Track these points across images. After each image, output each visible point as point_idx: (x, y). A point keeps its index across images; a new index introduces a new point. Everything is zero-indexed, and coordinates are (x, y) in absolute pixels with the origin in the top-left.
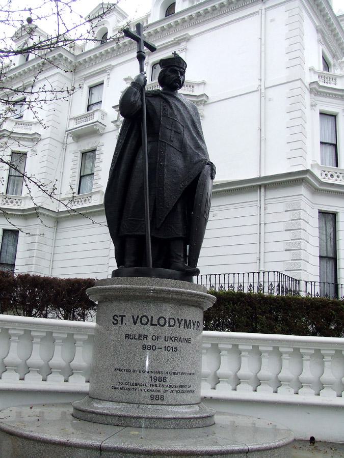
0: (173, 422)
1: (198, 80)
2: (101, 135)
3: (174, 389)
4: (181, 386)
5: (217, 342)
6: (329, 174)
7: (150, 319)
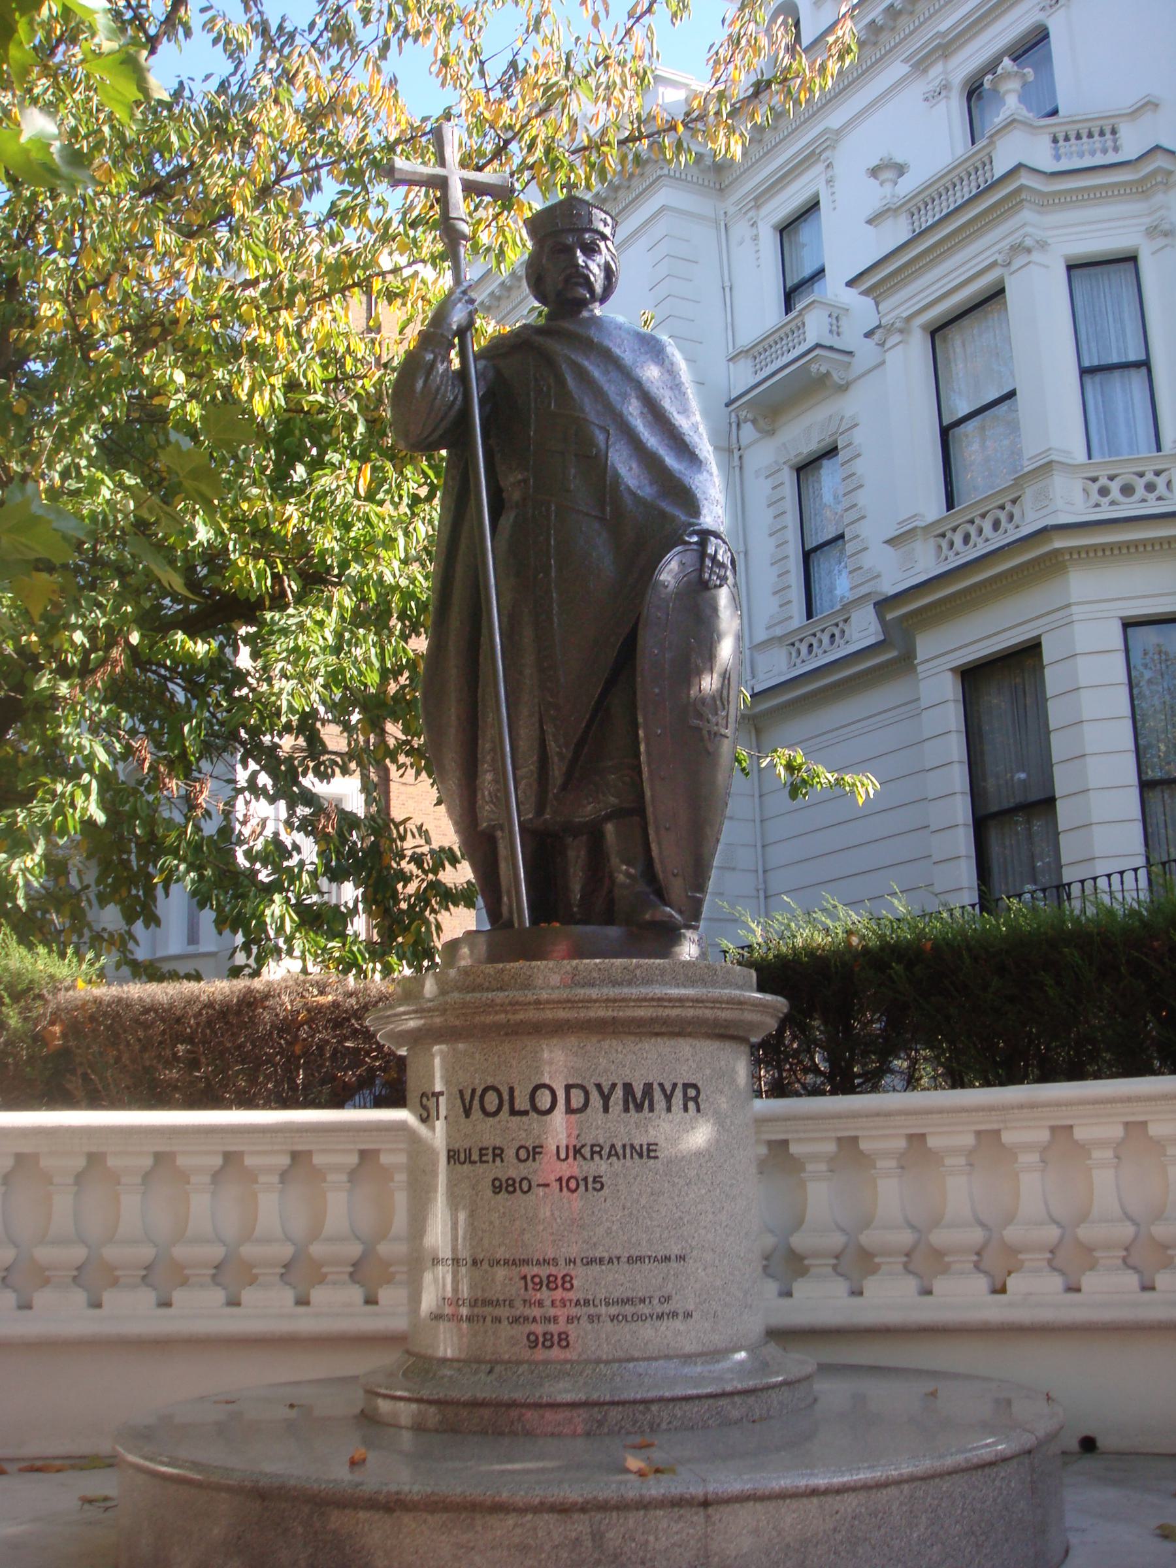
0: (583, 1413)
1: (1127, 100)
2: (844, 388)
3: (603, 1310)
4: (628, 1301)
6: (1115, 487)
7: (506, 1097)
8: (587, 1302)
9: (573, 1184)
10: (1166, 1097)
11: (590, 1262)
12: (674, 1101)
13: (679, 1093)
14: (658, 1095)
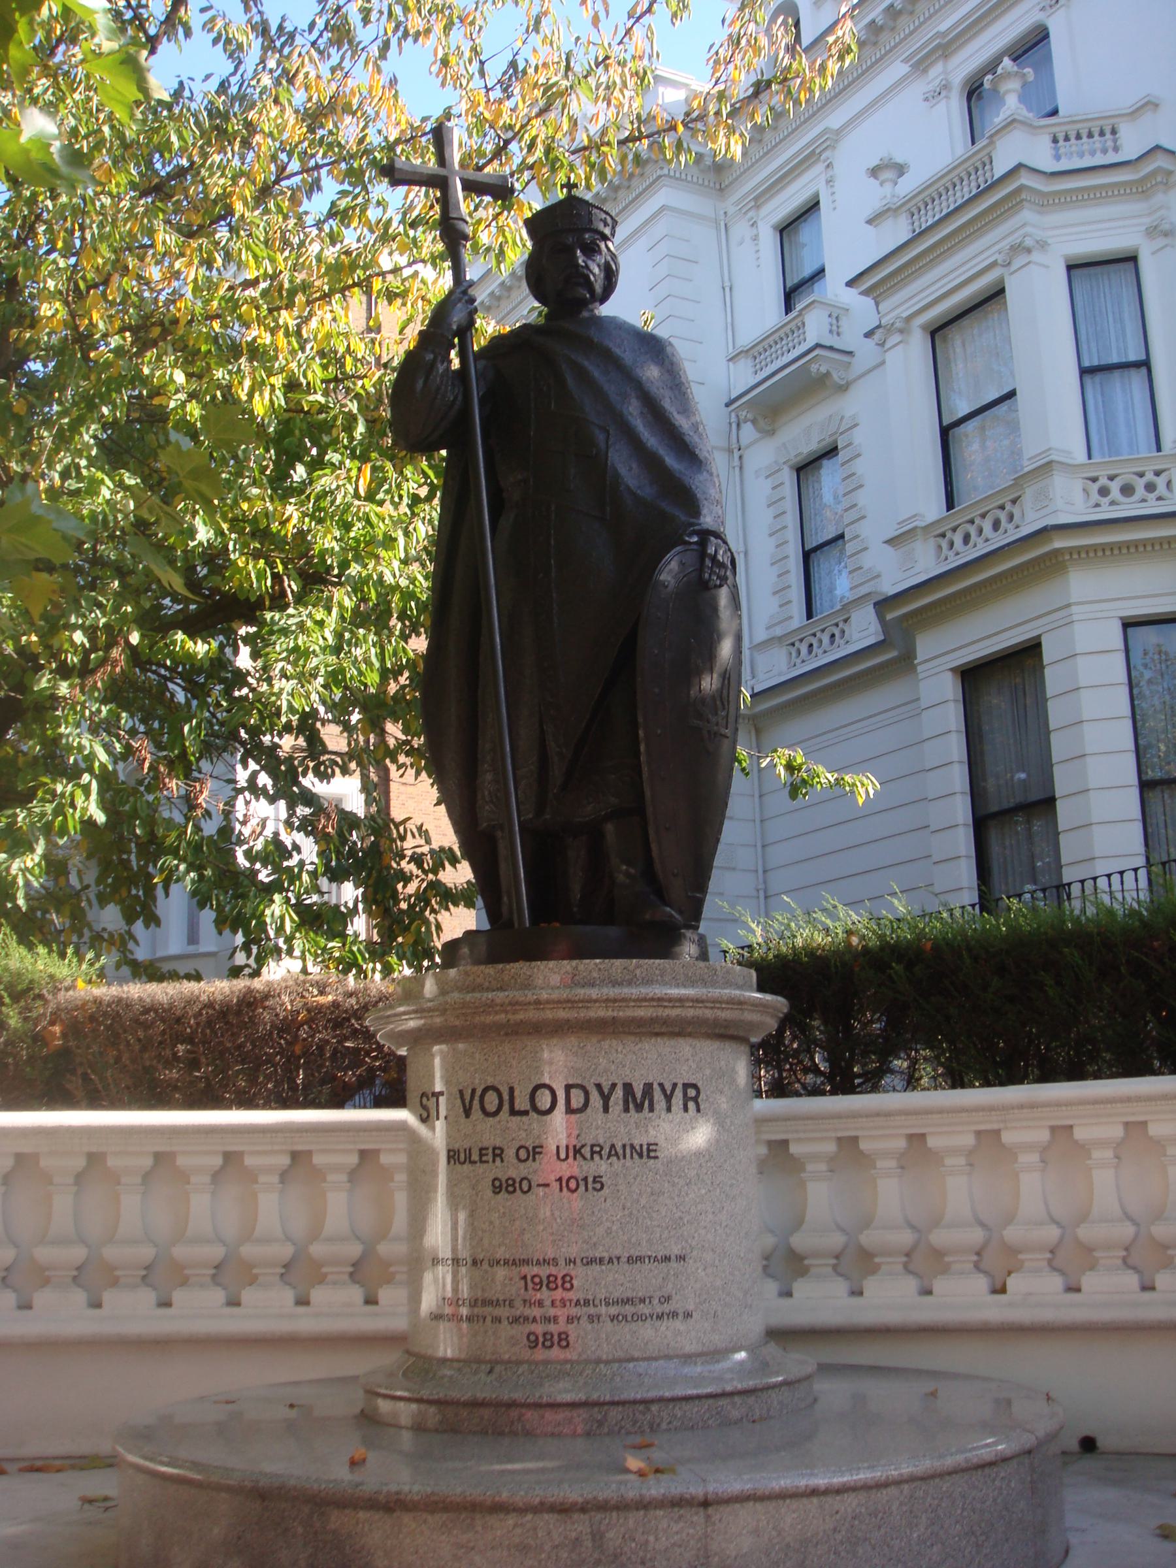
0: (583, 1413)
1: (1127, 100)
2: (844, 388)
3: (603, 1310)
4: (628, 1301)
5: (995, 1126)
6: (1115, 487)
7: (506, 1097)
8: (587, 1303)
9: (573, 1184)
10: (1166, 1097)
11: (590, 1262)
12: (674, 1101)
13: (679, 1093)
14: (658, 1095)
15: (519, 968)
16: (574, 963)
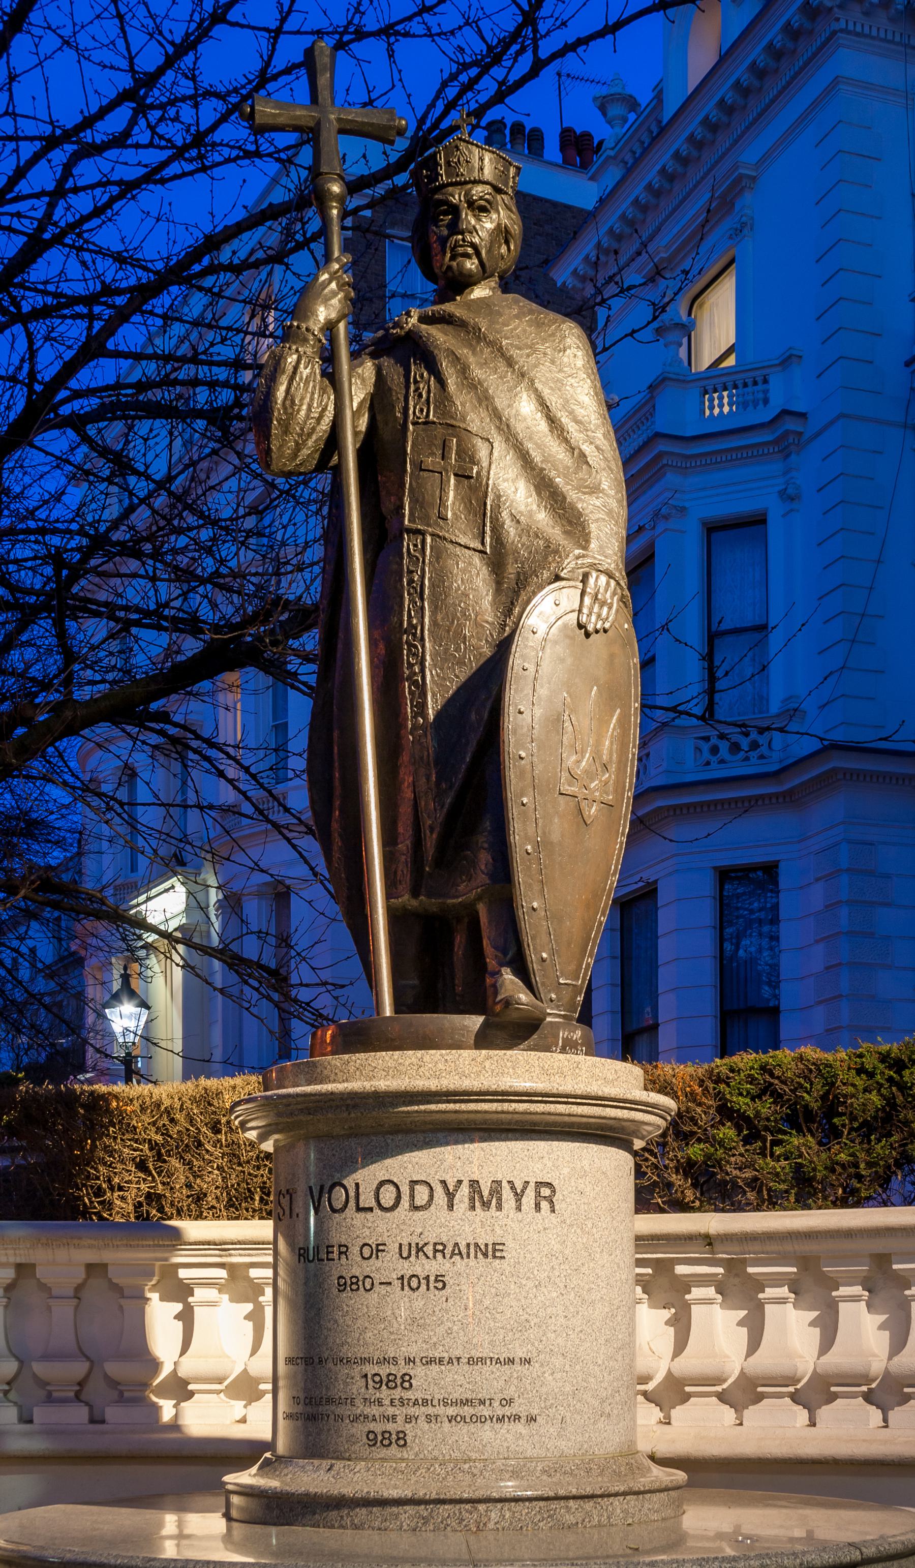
3: (440, 1410)
7: (352, 1194)
8: (425, 1402)
9: (414, 1283)
11: (430, 1361)
12: (524, 1200)
13: (530, 1193)
14: (507, 1193)
15: (360, 1058)
16: (419, 1053)
